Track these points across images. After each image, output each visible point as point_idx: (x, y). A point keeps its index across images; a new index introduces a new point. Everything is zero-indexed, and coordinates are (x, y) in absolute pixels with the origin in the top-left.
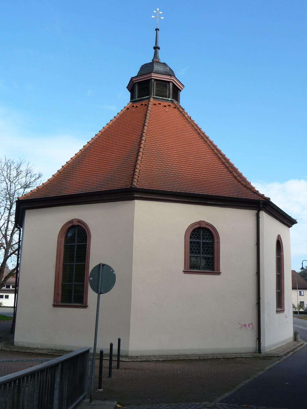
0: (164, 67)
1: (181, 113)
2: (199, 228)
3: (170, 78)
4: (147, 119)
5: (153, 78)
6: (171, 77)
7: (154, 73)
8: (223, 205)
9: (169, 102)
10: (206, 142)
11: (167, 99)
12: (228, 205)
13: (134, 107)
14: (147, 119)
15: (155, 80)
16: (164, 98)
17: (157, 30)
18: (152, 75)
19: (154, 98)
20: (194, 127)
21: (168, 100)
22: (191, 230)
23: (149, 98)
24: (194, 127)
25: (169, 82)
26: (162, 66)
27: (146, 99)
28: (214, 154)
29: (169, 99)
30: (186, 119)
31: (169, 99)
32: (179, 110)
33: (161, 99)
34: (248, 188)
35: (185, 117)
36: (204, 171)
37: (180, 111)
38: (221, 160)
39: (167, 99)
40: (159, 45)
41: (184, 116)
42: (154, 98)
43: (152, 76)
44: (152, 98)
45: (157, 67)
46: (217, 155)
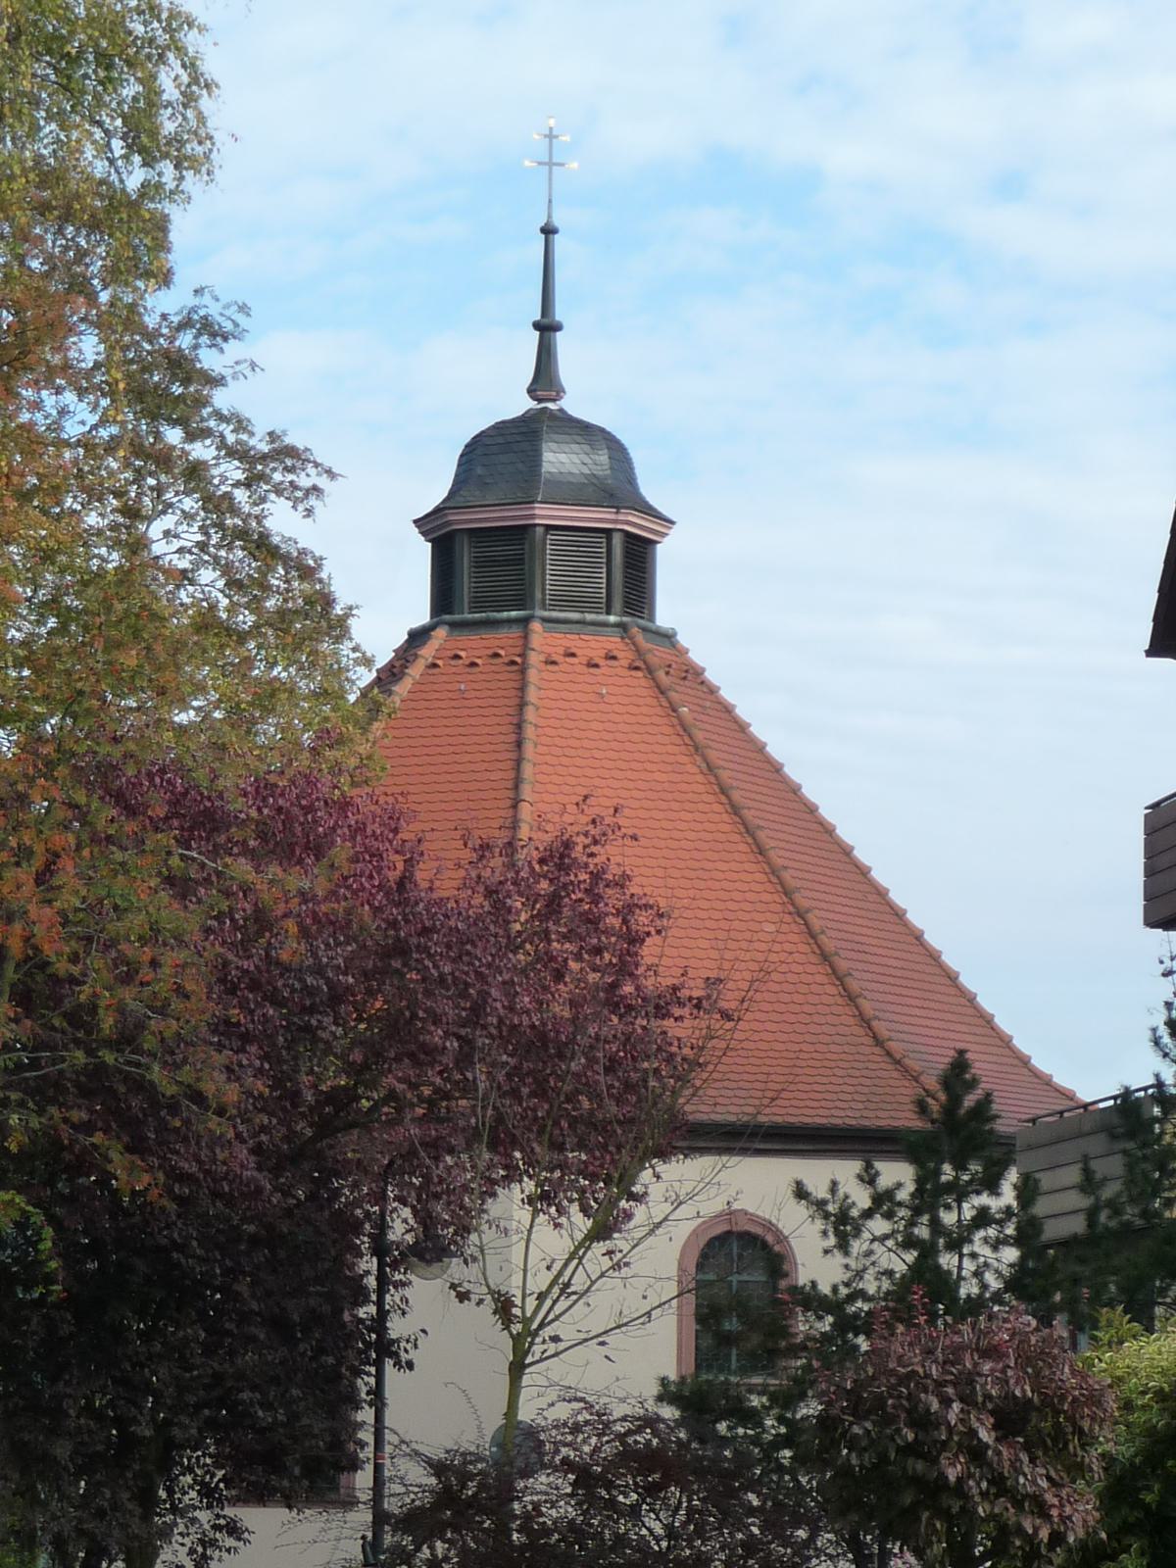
0: (586, 448)
1: (662, 693)
2: (723, 1239)
3: (613, 517)
4: (529, 761)
5: (537, 521)
6: (617, 513)
7: (541, 502)
8: (814, 1151)
9: (609, 629)
10: (760, 854)
11: (602, 618)
12: (825, 1151)
13: (461, 662)
14: (529, 761)
15: (549, 528)
16: (589, 617)
17: (548, 231)
18: (537, 512)
19: (545, 620)
20: (716, 776)
21: (605, 624)
22: (702, 1243)
23: (525, 622)
24: (716, 776)
25: (608, 532)
26: (575, 447)
27: (510, 621)
28: (790, 913)
29: (612, 619)
30: (682, 733)
31: (612, 619)
32: (653, 679)
33: (578, 622)
34: (907, 1071)
35: (679, 718)
36: (752, 1060)
37: (658, 687)
38: (816, 943)
39: (602, 618)
40: (559, 315)
41: (674, 711)
42: (545, 620)
43: (533, 516)
44: (536, 626)
45: (558, 459)
46: (803, 919)
